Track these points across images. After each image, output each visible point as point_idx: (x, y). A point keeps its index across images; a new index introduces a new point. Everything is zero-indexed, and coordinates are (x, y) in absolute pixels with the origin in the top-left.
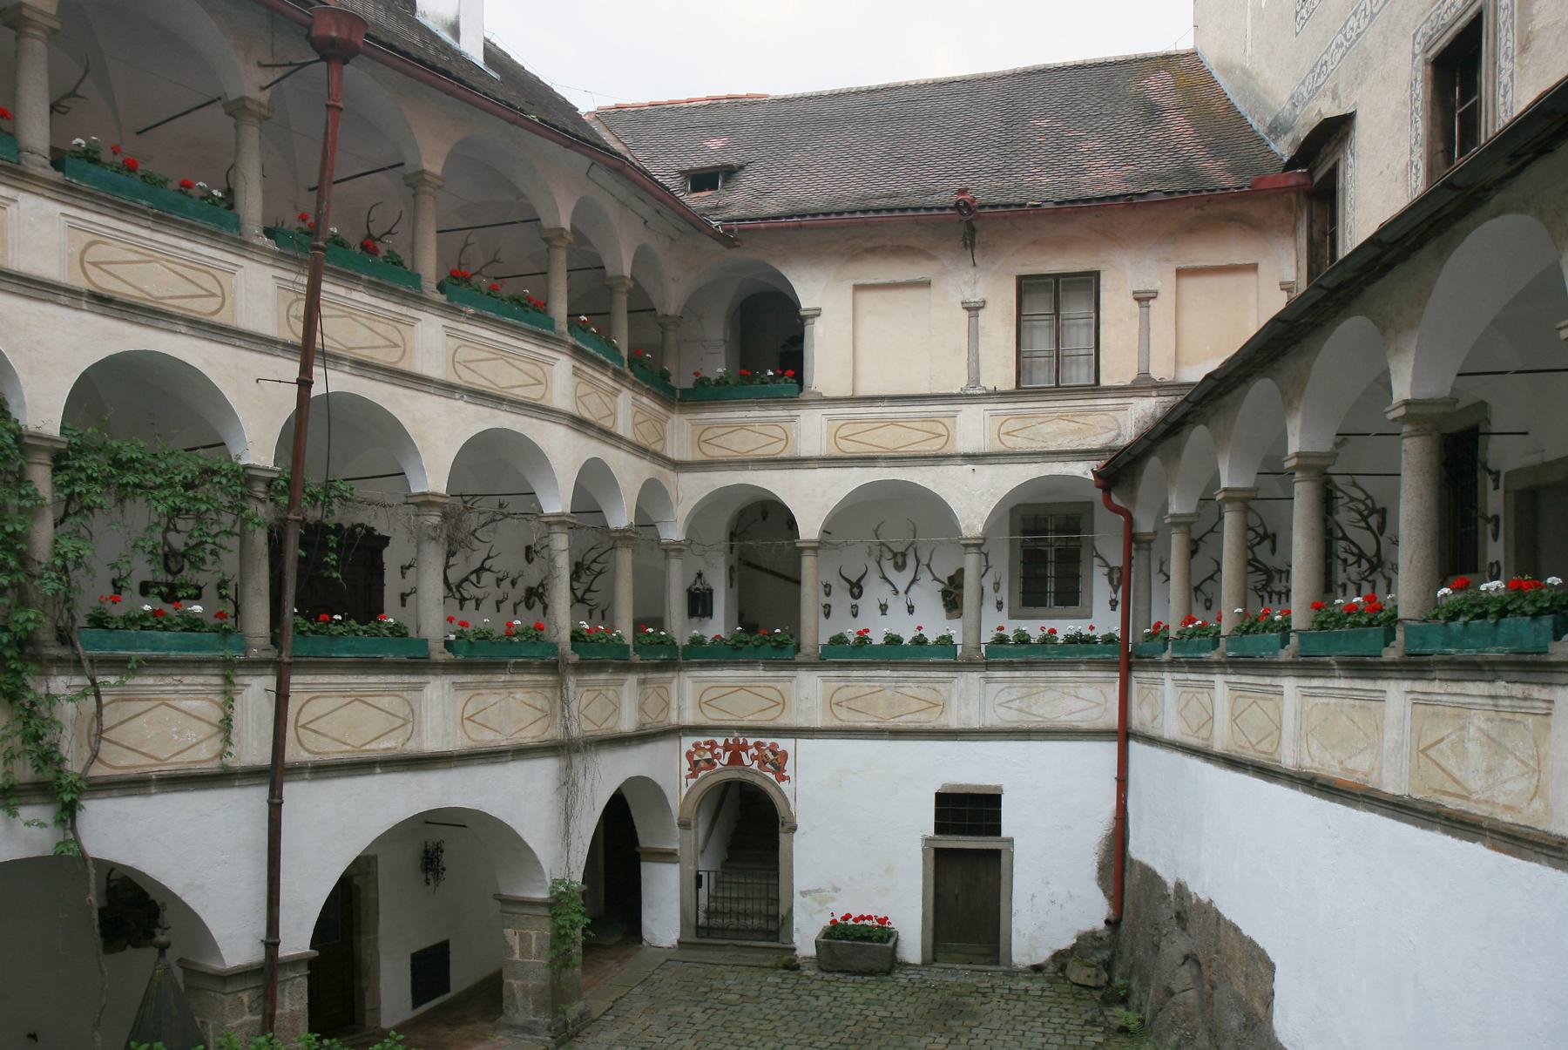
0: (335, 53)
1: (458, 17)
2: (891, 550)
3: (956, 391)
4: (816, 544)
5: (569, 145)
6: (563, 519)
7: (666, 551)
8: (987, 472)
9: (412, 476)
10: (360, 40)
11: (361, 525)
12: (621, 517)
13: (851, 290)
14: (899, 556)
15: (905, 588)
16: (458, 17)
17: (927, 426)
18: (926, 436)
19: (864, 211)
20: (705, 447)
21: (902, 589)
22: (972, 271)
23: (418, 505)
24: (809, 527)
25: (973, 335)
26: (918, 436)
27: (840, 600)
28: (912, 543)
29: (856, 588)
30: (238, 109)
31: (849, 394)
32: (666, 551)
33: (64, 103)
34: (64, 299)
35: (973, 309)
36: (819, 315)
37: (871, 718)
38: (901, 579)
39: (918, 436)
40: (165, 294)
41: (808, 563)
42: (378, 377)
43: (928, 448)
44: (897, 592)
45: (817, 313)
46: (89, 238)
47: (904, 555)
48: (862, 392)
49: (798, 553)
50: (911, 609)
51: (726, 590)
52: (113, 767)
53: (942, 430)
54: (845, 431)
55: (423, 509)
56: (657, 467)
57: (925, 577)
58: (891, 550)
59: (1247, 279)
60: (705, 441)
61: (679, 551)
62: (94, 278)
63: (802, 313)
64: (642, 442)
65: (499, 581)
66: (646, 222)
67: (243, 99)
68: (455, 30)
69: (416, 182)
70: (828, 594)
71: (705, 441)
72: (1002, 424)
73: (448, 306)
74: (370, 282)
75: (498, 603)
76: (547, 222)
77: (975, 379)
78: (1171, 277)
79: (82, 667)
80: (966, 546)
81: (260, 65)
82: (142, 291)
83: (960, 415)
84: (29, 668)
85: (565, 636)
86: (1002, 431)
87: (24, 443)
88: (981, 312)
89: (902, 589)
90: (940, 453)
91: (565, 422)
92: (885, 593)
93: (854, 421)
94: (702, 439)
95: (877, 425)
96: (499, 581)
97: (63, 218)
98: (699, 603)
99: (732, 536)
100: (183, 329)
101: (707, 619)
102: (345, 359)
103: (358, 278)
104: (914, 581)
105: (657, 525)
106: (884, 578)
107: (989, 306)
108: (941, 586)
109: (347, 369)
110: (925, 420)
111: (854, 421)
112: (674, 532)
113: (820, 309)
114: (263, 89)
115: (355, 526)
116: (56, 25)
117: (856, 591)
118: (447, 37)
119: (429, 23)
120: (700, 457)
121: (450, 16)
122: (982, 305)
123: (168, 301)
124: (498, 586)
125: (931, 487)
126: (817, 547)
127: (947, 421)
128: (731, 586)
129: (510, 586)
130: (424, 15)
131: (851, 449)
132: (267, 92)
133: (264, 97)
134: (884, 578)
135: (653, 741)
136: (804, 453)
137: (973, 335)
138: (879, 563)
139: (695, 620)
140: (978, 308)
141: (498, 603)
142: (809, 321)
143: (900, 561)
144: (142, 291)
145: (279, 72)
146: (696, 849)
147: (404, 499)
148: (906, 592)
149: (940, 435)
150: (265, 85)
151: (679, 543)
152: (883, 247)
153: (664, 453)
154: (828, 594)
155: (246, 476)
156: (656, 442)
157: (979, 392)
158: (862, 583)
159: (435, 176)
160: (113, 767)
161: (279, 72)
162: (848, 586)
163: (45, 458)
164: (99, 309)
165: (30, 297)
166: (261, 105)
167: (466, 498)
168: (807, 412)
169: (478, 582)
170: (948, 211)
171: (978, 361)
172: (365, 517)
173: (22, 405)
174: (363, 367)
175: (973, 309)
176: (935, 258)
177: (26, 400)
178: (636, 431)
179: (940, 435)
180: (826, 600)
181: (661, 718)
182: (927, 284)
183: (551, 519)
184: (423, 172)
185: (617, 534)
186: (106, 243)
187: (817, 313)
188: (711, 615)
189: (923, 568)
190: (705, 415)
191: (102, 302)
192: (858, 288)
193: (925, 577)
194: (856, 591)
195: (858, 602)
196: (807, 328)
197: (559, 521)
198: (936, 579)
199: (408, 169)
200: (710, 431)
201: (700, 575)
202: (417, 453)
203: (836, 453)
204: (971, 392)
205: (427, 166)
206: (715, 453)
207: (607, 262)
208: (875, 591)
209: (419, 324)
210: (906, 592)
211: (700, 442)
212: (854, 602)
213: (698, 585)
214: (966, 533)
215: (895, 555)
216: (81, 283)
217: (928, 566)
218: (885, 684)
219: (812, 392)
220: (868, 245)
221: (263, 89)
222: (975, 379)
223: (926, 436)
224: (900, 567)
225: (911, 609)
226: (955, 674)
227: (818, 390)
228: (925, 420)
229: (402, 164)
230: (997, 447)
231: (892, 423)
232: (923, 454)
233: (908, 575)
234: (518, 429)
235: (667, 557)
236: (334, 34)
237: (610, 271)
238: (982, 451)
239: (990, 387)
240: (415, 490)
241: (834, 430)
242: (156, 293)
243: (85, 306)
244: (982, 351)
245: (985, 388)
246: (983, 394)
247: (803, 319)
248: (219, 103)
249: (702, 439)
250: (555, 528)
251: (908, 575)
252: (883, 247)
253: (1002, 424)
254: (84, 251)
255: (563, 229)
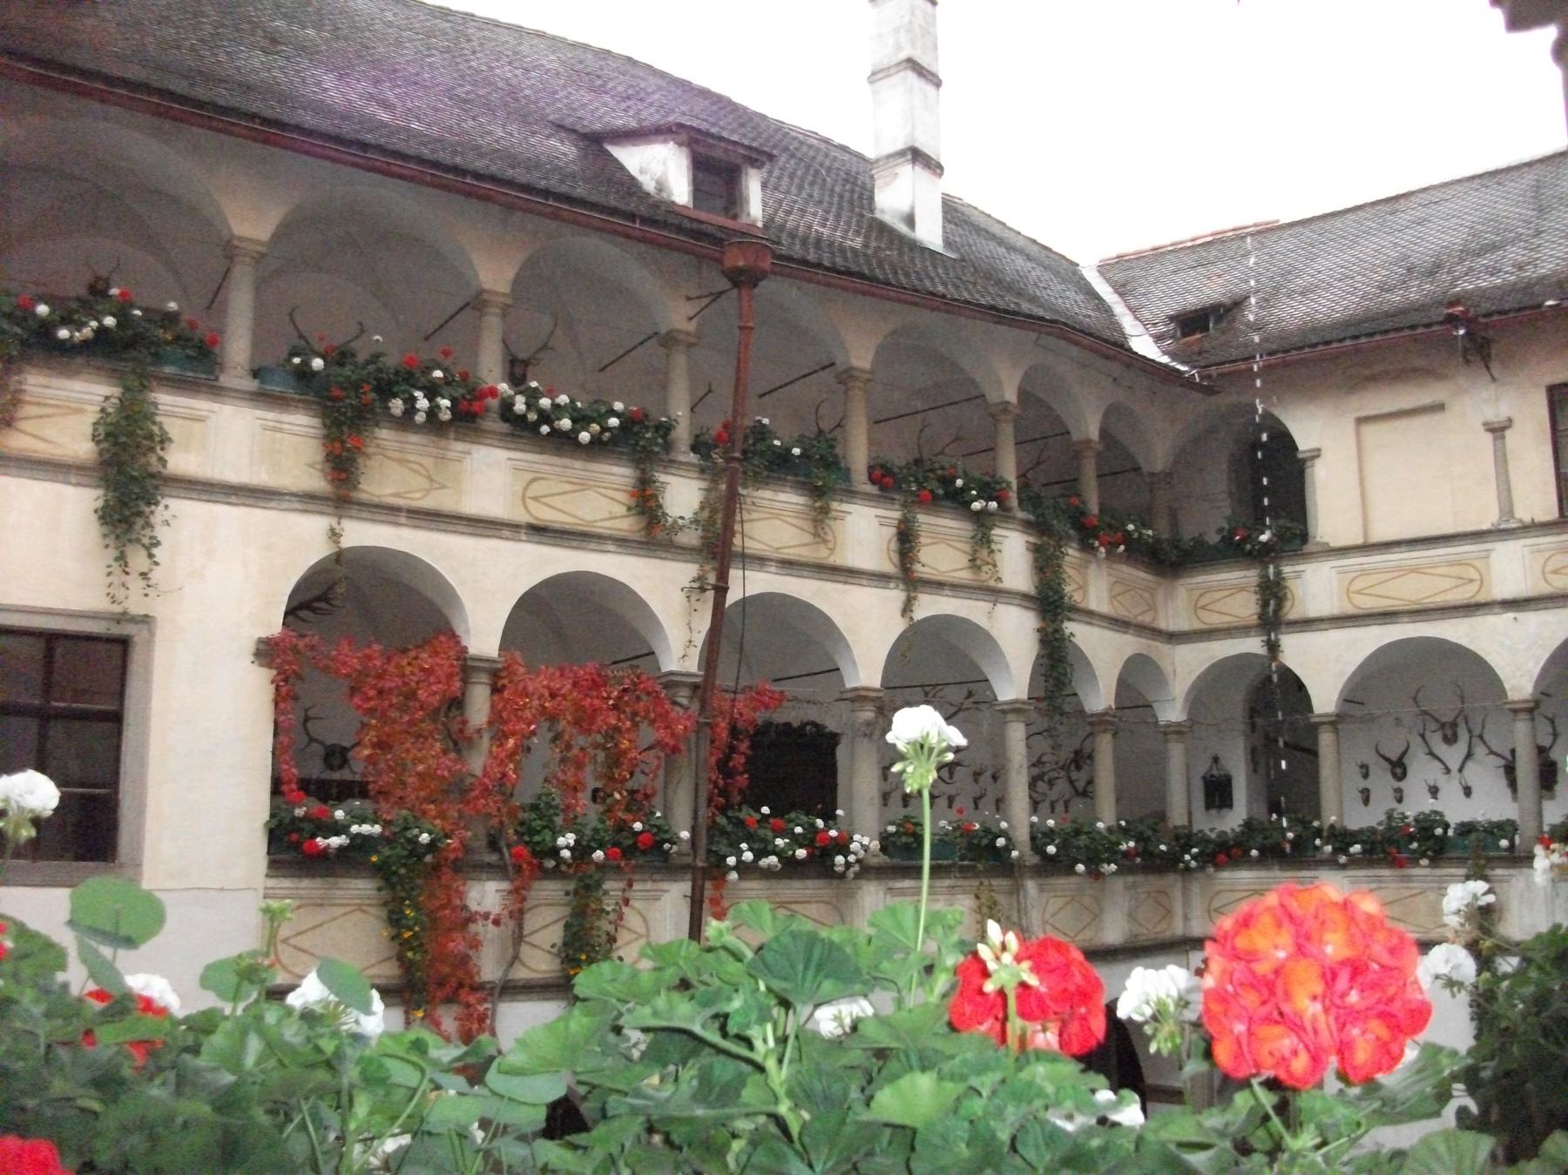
0: (744, 279)
1: (913, 208)
2: (1437, 720)
3: (1485, 527)
4: (1333, 719)
5: (999, 321)
6: (1017, 706)
7: (1165, 734)
8: (1533, 620)
9: (846, 671)
10: (767, 264)
11: (815, 724)
12: (1100, 697)
13: (1351, 426)
14: (1447, 727)
15: (1458, 766)
16: (913, 208)
17: (1455, 570)
18: (1454, 582)
19: (1427, 326)
20: (1202, 614)
21: (1454, 767)
22: (1492, 387)
23: (853, 700)
24: (1324, 698)
25: (1501, 460)
26: (1446, 583)
27: (1382, 783)
28: (1461, 711)
29: (1399, 768)
30: (669, 341)
31: (1360, 541)
32: (1165, 734)
33: (537, 356)
34: (506, 533)
35: (1498, 430)
36: (1318, 456)
37: (1411, 928)
38: (1453, 755)
39: (1446, 583)
40: (598, 518)
41: (1326, 740)
42: (805, 573)
43: (1459, 597)
44: (1448, 771)
45: (1316, 454)
46: (529, 476)
47: (1454, 725)
48: (1378, 536)
49: (1313, 729)
50: (1468, 791)
51: (1248, 777)
52: (535, 971)
53: (1472, 574)
54: (1358, 585)
55: (857, 704)
56: (1144, 641)
57: (1480, 750)
58: (1437, 720)
59: (1436, 418)
60: (1203, 608)
61: (1178, 733)
62: (533, 511)
63: (1300, 456)
64: (1122, 613)
65: (977, 775)
66: (1115, 380)
67: (671, 331)
68: (910, 220)
69: (847, 377)
70: (1366, 776)
71: (1203, 608)
72: (1547, 560)
73: (879, 496)
74: (798, 482)
75: (976, 801)
76: (992, 397)
77: (1507, 509)
78: (1350, 427)
79: (507, 872)
80: (1515, 711)
81: (689, 298)
82: (576, 517)
83: (1494, 555)
84: (636, 886)
85: (1022, 835)
86: (1549, 568)
87: (467, 667)
88: (1508, 433)
89: (1454, 767)
90: (1473, 601)
91: (1017, 602)
92: (1433, 772)
93: (1365, 573)
94: (1200, 605)
95: (1395, 574)
96: (977, 775)
97: (509, 463)
98: (1218, 792)
99: (1253, 712)
100: (611, 548)
101: (1225, 811)
102: (771, 560)
103: (785, 480)
104: (1469, 756)
105: (1154, 705)
106: (1431, 754)
107: (1517, 425)
108: (1503, 762)
109: (773, 569)
110: (1451, 564)
111: (1365, 573)
112: (1172, 712)
113: (1319, 450)
114: (690, 319)
115: (804, 725)
116: (509, 301)
117: (1399, 771)
118: (902, 228)
119: (888, 218)
120: (1197, 626)
121: (904, 207)
122: (1506, 424)
123: (600, 524)
124: (976, 781)
125: (1464, 642)
126: (1336, 722)
127: (1478, 564)
128: (1255, 771)
129: (990, 780)
130: (882, 211)
131: (1368, 604)
132: (694, 322)
133: (691, 327)
134: (1431, 754)
135: (1146, 957)
136: (1313, 614)
137: (1501, 460)
138: (1423, 736)
139: (1213, 812)
140: (1503, 429)
141: (976, 801)
142: (1309, 463)
143: (1449, 733)
144: (576, 517)
145: (705, 301)
146: (1211, 1088)
147: (837, 696)
148: (1461, 770)
149: (1471, 581)
150: (691, 315)
151: (1179, 724)
152: (1387, 372)
153: (1153, 625)
154: (1366, 776)
155: (672, 682)
156: (1144, 612)
157: (1514, 526)
158: (1405, 761)
159: (862, 371)
160: (535, 971)
161: (705, 301)
162: (1387, 765)
163: (484, 678)
164: (536, 538)
165: (476, 535)
166: (688, 334)
167: (927, 689)
168: (1314, 566)
169: (951, 778)
170: (1435, 328)
171: (1509, 491)
172: (812, 714)
173: (467, 631)
174: (789, 565)
175: (1498, 430)
176: (1446, 377)
177: (471, 626)
178: (1116, 603)
179: (1471, 581)
180: (1363, 784)
181: (1158, 929)
182: (1439, 408)
183: (1005, 707)
184: (851, 368)
185: (1094, 719)
186: (543, 479)
187: (1316, 454)
188: (1230, 806)
189: (1476, 741)
190: (1201, 579)
191: (540, 532)
192: (1362, 421)
193: (1480, 750)
194: (1399, 771)
195: (1402, 784)
196: (1308, 471)
197: (1015, 709)
198: (1492, 752)
199: (840, 368)
200: (1208, 595)
201: (1216, 760)
202: (848, 646)
203: (1350, 610)
204: (1503, 526)
205: (855, 362)
206: (1215, 620)
207: (1070, 424)
208: (1422, 771)
209: (849, 518)
210: (1461, 770)
211: (1197, 608)
212: (1397, 784)
213: (1215, 772)
214: (1513, 695)
215: (1443, 726)
216: (522, 517)
217: (1481, 737)
218: (1426, 885)
219: (1318, 543)
220: (1367, 372)
221: (690, 319)
222: (1507, 509)
223: (1454, 582)
224: (1450, 740)
225: (1468, 791)
226: (1512, 872)
227: (1325, 540)
228: (1451, 564)
229: (833, 364)
230: (1543, 589)
231: (1413, 571)
232: (1451, 604)
233: (1460, 749)
234: (962, 614)
235: (1166, 741)
236: (741, 263)
237: (1076, 436)
238: (1531, 594)
239: (1527, 519)
240: (849, 685)
241: (1346, 584)
242: (589, 517)
243: (524, 537)
244: (1512, 475)
245: (1521, 521)
246: (1518, 528)
247: (1304, 461)
248: (654, 340)
249: (1200, 605)
250: (1010, 717)
251: (1460, 749)
252: (1387, 372)
253: (1547, 560)
254: (525, 489)
255: (1008, 403)
